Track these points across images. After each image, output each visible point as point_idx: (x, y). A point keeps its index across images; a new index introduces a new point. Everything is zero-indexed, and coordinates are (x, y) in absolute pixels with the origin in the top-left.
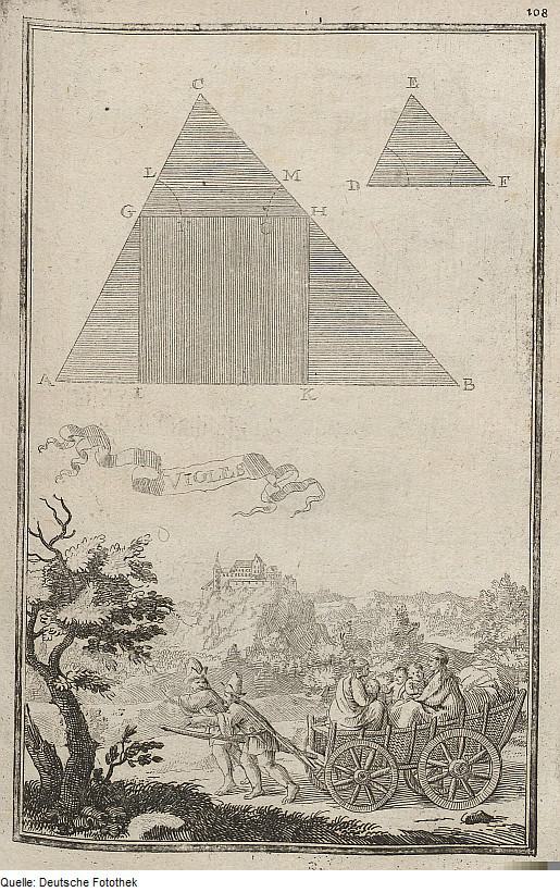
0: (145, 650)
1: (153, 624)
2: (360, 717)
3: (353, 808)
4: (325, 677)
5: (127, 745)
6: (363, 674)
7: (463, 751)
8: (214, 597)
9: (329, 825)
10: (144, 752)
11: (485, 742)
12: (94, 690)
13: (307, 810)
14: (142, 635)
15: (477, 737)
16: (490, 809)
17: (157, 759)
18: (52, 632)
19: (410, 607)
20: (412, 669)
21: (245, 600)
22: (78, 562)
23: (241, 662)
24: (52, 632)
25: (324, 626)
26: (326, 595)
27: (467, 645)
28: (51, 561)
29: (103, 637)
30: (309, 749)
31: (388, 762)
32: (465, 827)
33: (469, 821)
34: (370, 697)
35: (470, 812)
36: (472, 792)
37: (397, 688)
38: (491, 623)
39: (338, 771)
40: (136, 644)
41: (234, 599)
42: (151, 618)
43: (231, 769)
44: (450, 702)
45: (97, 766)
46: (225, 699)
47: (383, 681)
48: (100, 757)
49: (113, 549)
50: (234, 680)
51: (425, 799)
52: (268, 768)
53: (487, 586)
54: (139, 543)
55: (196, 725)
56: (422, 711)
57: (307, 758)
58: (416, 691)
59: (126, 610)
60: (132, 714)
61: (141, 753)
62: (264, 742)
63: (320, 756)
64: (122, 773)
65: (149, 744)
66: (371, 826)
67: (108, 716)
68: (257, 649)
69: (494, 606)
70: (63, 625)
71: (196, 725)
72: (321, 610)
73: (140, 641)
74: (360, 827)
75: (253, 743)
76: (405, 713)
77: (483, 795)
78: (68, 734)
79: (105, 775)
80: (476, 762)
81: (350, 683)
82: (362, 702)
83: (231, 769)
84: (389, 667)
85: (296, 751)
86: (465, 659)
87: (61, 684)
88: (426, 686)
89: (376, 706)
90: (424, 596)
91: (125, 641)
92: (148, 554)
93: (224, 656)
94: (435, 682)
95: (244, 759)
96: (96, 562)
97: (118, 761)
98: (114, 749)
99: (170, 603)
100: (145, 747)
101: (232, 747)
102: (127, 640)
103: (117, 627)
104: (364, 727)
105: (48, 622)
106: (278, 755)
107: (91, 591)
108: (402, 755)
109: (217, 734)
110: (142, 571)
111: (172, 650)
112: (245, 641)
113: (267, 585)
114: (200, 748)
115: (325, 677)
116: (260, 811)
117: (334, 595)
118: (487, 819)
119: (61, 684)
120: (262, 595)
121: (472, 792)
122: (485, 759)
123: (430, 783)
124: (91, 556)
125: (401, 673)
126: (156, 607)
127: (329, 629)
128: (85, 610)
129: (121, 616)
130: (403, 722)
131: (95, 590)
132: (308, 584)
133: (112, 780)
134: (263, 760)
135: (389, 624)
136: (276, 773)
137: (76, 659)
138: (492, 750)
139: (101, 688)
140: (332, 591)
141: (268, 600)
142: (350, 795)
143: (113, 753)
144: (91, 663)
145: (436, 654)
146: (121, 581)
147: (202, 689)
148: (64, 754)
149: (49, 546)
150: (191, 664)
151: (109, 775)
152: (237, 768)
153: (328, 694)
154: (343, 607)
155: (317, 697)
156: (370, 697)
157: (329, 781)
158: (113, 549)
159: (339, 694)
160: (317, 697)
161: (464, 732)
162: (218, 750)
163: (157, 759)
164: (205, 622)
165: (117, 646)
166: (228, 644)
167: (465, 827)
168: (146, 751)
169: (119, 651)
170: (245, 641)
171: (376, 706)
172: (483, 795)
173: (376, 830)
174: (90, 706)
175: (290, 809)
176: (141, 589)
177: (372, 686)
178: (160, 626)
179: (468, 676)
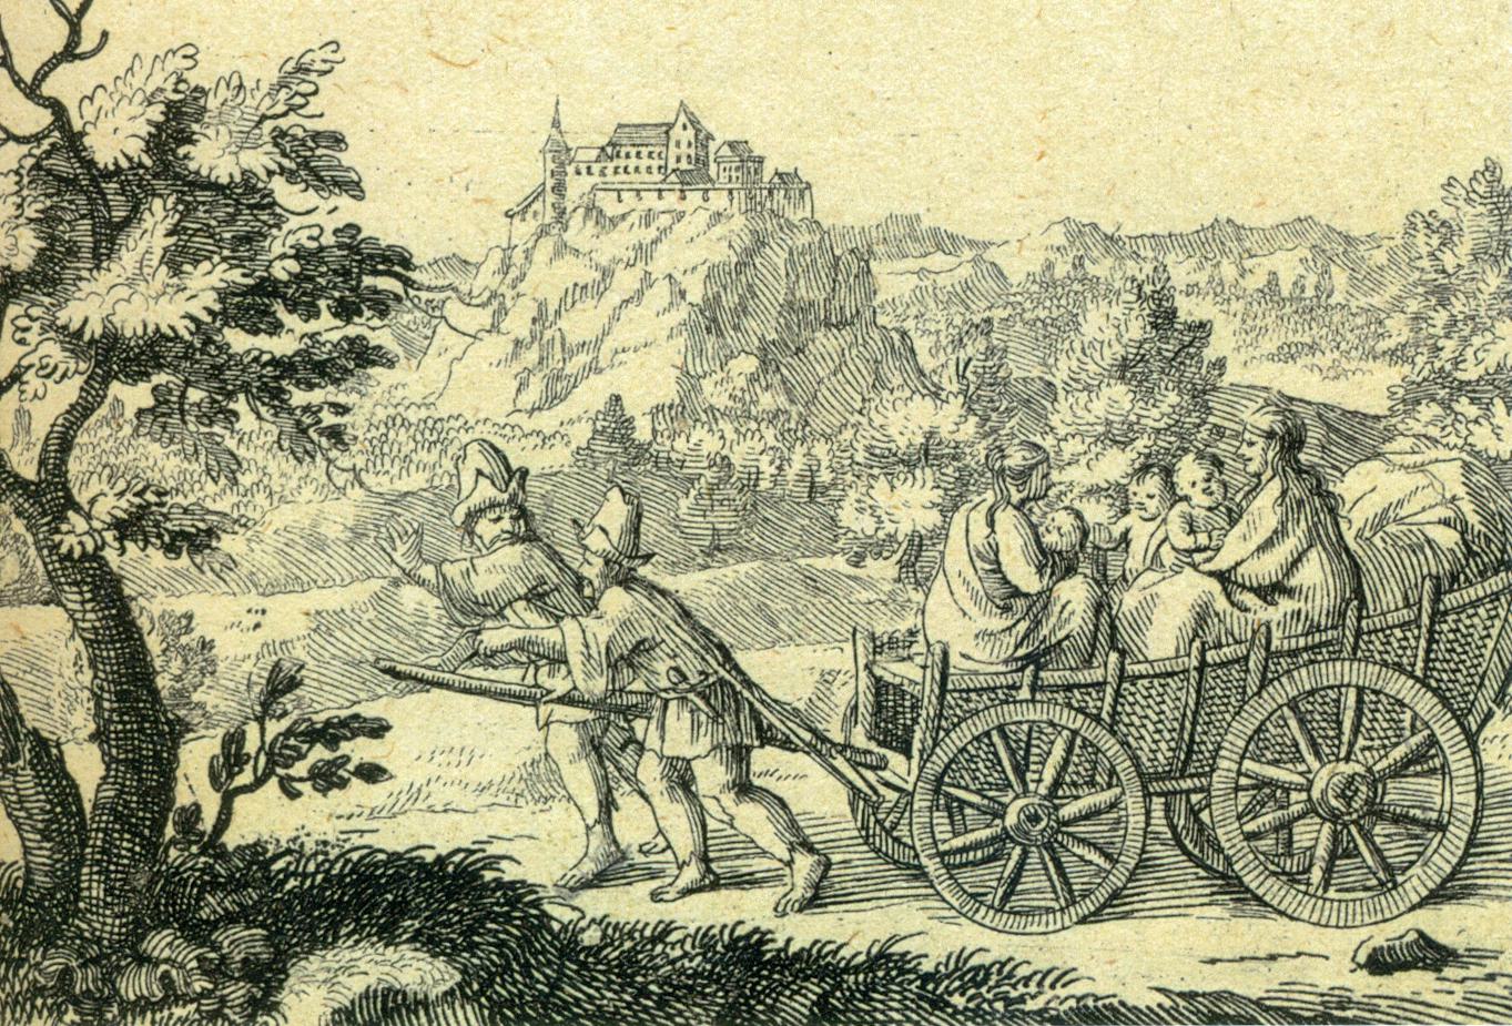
0: (328, 419)
1: (352, 331)
2: (1023, 627)
3: (1001, 920)
4: (911, 504)
5: (274, 728)
6: (1027, 485)
7: (1356, 731)
8: (547, 246)
9: (926, 978)
10: (326, 748)
11: (1426, 704)
12: (171, 549)
13: (852, 930)
14: (314, 367)
15: (1402, 687)
16: (1445, 924)
17: (371, 773)
18: (47, 372)
19: (1181, 272)
20: (1190, 472)
21: (644, 252)
22: (116, 139)
23: (639, 454)
24: (47, 372)
25: (904, 334)
26: (912, 236)
27: (1368, 389)
28: (37, 138)
29: (187, 374)
30: (860, 739)
31: (1112, 773)
32: (1364, 984)
33: (1379, 964)
34: (1056, 564)
35: (1381, 936)
36: (1388, 868)
37: (1141, 534)
38: (1441, 318)
39: (954, 808)
40: (299, 397)
41: (616, 244)
42: (346, 311)
43: (608, 805)
44: (1314, 573)
45: (183, 798)
46: (587, 571)
47: (1096, 512)
48: (196, 757)
49: (223, 93)
50: (615, 513)
51: (1232, 888)
52: (728, 799)
53: (1429, 199)
54: (302, 69)
55: (489, 658)
56: (1221, 604)
57: (855, 765)
58: (1203, 539)
59: (267, 288)
60: (288, 618)
61: (319, 753)
62: (716, 717)
63: (896, 760)
64: (263, 817)
65: (343, 723)
66: (1064, 977)
67: (219, 628)
68: (680, 412)
69: (1449, 261)
70: (73, 339)
71: (489, 658)
72: (893, 281)
73: (311, 386)
74: (1027, 980)
75: (678, 722)
76: (1165, 613)
77: (1417, 882)
78: (98, 699)
79: (208, 823)
80: (1399, 771)
81: (991, 523)
82: (1025, 577)
83: (608, 805)
84: (1114, 465)
85: (820, 746)
86: (1358, 435)
87: (75, 534)
88: (1233, 523)
89: (1075, 594)
90: (1217, 238)
91: (264, 388)
92: (332, 108)
93: (581, 434)
94: (1265, 510)
95: (650, 772)
96: (177, 122)
97: (246, 777)
98: (234, 740)
99: (406, 263)
100: (330, 733)
101: (611, 729)
102: (271, 383)
103: (238, 341)
104: (1036, 660)
105: (33, 337)
106: (764, 759)
107: (158, 219)
108: (1158, 751)
109: (560, 685)
110: (315, 160)
111: (413, 416)
112: (645, 383)
113: (719, 201)
114: (498, 736)
115: (911, 504)
116: (705, 940)
117: (935, 232)
118: (1432, 955)
119: (75, 534)
120: (700, 239)
121: (1388, 868)
122: (1424, 758)
123: (1250, 837)
124: (156, 113)
125: (1153, 483)
126: (361, 274)
127: (922, 345)
128: (139, 290)
129: (253, 304)
130: (1162, 639)
131: (171, 221)
132: (847, 201)
133: (231, 839)
134: (712, 776)
135: (1111, 326)
136: (753, 819)
137: (123, 455)
138: (1448, 734)
139: (194, 541)
140: (926, 223)
141: (722, 254)
142: (989, 878)
143: (232, 755)
144: (160, 461)
145: (1265, 421)
146: (248, 195)
147: (515, 538)
148: (86, 767)
149: (32, 91)
150: (476, 459)
151: (223, 822)
152: (627, 802)
153: (917, 559)
154: (965, 271)
155: (882, 570)
156: (1056, 564)
157: (926, 829)
158: (223, 93)
159: (956, 557)
160: (882, 570)
161: (1368, 674)
162: (565, 741)
163: (371, 773)
164: (518, 324)
165: (240, 405)
166: (590, 396)
167: (1364, 984)
168: (333, 743)
169: (247, 421)
170: (645, 383)
171: (1075, 594)
172: (1417, 882)
173: (1078, 989)
174: (156, 608)
175: (801, 932)
176: (307, 215)
177: (1059, 531)
178: (375, 339)
179: (1366, 489)
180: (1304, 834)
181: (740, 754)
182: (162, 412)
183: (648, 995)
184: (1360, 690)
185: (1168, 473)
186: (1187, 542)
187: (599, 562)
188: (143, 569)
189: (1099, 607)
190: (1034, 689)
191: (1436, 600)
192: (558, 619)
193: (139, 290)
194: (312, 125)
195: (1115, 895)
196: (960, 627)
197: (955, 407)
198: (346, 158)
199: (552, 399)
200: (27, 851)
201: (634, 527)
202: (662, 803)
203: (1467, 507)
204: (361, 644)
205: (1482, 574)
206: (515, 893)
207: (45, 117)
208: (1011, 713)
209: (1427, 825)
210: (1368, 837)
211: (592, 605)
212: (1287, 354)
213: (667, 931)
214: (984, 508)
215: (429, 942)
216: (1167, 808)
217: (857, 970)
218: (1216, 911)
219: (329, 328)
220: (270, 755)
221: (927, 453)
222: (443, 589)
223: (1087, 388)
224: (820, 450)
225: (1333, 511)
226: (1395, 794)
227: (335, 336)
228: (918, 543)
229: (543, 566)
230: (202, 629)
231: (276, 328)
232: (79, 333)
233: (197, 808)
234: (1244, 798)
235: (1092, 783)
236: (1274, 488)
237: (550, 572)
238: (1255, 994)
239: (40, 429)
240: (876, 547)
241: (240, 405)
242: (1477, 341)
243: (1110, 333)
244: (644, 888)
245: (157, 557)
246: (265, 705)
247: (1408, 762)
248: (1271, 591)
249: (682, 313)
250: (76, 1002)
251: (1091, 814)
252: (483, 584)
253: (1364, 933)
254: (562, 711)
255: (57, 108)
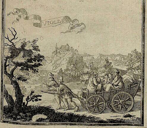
4: (86, 77)
5: (32, 96)
6: (96, 76)
7: (123, 97)
8: (56, 55)
9: (87, 118)
11: (130, 95)
12: (23, 81)
13: (81, 114)
14: (36, 66)
15: (127, 94)
16: (131, 113)
17: (40, 100)
18: (11, 65)
19: (109, 58)
20: (110, 75)
22: (18, 46)
24: (11, 65)
25: (86, 63)
26: (86, 55)
27: (125, 69)
28: (11, 45)
29: (25, 66)
31: (103, 101)
35: (125, 114)
36: (126, 109)
38: (131, 62)
39: (89, 103)
40: (34, 68)
42: (38, 61)
43: (60, 103)
44: (120, 84)
45: (23, 102)
46: (59, 83)
47: (102, 78)
50: (61, 78)
51: (113, 111)
52: (70, 102)
53: (130, 52)
56: (112, 87)
59: (31, 59)
60: (33, 87)
61: (36, 98)
62: (69, 95)
64: (30, 103)
65: (38, 96)
66: (99, 118)
67: (27, 88)
68: (67, 70)
72: (85, 59)
73: (35, 67)
74: (95, 118)
75: (66, 95)
76: (108, 87)
77: (129, 109)
78: (16, 93)
79: (26, 104)
80: (127, 101)
82: (96, 84)
83: (60, 103)
84: (103, 74)
85: (78, 98)
86: (124, 72)
88: (113, 80)
89: (100, 85)
92: (37, 44)
93: (58, 72)
94: (116, 79)
95: (64, 100)
97: (29, 100)
98: (28, 97)
100: (37, 96)
101: (60, 96)
102: (32, 67)
103: (29, 63)
104: (97, 91)
106: (73, 99)
107: (22, 54)
108: (107, 99)
110: (36, 48)
112: (64, 68)
113: (70, 52)
114: (52, 97)
115: (86, 77)
116: (68, 114)
117: (88, 55)
118: (130, 116)
119: (14, 79)
120: (69, 55)
121: (126, 109)
122: (129, 99)
123: (114, 106)
125: (107, 76)
126: (40, 58)
128: (20, 59)
129: (30, 61)
130: (107, 90)
131: (23, 53)
133: (28, 105)
134: (69, 100)
135: (103, 63)
136: (72, 104)
137: (18, 72)
138: (131, 97)
139: (25, 80)
143: (28, 98)
144: (22, 73)
145: (116, 71)
148: (14, 98)
149: (10, 41)
151: (27, 104)
152: (62, 102)
155: (84, 83)
157: (87, 105)
159: (90, 82)
160: (84, 83)
161: (124, 92)
162: (57, 97)
163: (40, 100)
164: (53, 62)
165: (29, 69)
166: (59, 68)
168: (37, 97)
169: (30, 70)
170: (64, 68)
171: (100, 85)
172: (129, 109)
173: (100, 119)
175: (76, 113)
178: (41, 63)
179: (125, 77)
180: (119, 105)
181: (71, 98)
182: (22, 69)
183: (63, 118)
184: (124, 94)
185: (108, 75)
186: (109, 81)
187: (60, 82)
188: (20, 82)
189: (102, 87)
190: (96, 93)
191: (130, 86)
192: (56, 87)
193: (20, 59)
194: (36, 45)
195: (103, 111)
196: (90, 88)
197: (90, 69)
198: (39, 48)
199: (56, 69)
200: (8, 105)
201: (63, 79)
202: (65, 102)
203: (133, 79)
204: (39, 89)
205: (134, 84)
206: (52, 110)
207: (12, 44)
208: (94, 95)
209: (129, 105)
210: (124, 106)
211: (59, 86)
212: (118, 65)
213: (65, 113)
214: (92, 78)
215: (45, 114)
216: (108, 104)
217: (81, 117)
218: (112, 112)
219: (37, 62)
220: (31, 98)
221: (87, 73)
222: (46, 85)
223: (101, 68)
224: (78, 73)
225: (122, 79)
226: (127, 103)
227: (37, 63)
228: (87, 81)
229: (55, 83)
230: (25, 87)
231: (32, 62)
232: (15, 62)
233: (25, 103)
234: (114, 103)
235: (101, 102)
236: (117, 77)
237: (56, 83)
238: (115, 119)
239: (11, 70)
240: (83, 81)
241: (29, 69)
242: (134, 64)
243: (103, 63)
244: (63, 109)
245: (21, 81)
246: (31, 94)
247: (128, 100)
248: (117, 85)
249: (67, 61)
250: (13, 118)
251: (101, 104)
252: (49, 84)
253: (124, 114)
254: (56, 95)
255: (13, 43)
